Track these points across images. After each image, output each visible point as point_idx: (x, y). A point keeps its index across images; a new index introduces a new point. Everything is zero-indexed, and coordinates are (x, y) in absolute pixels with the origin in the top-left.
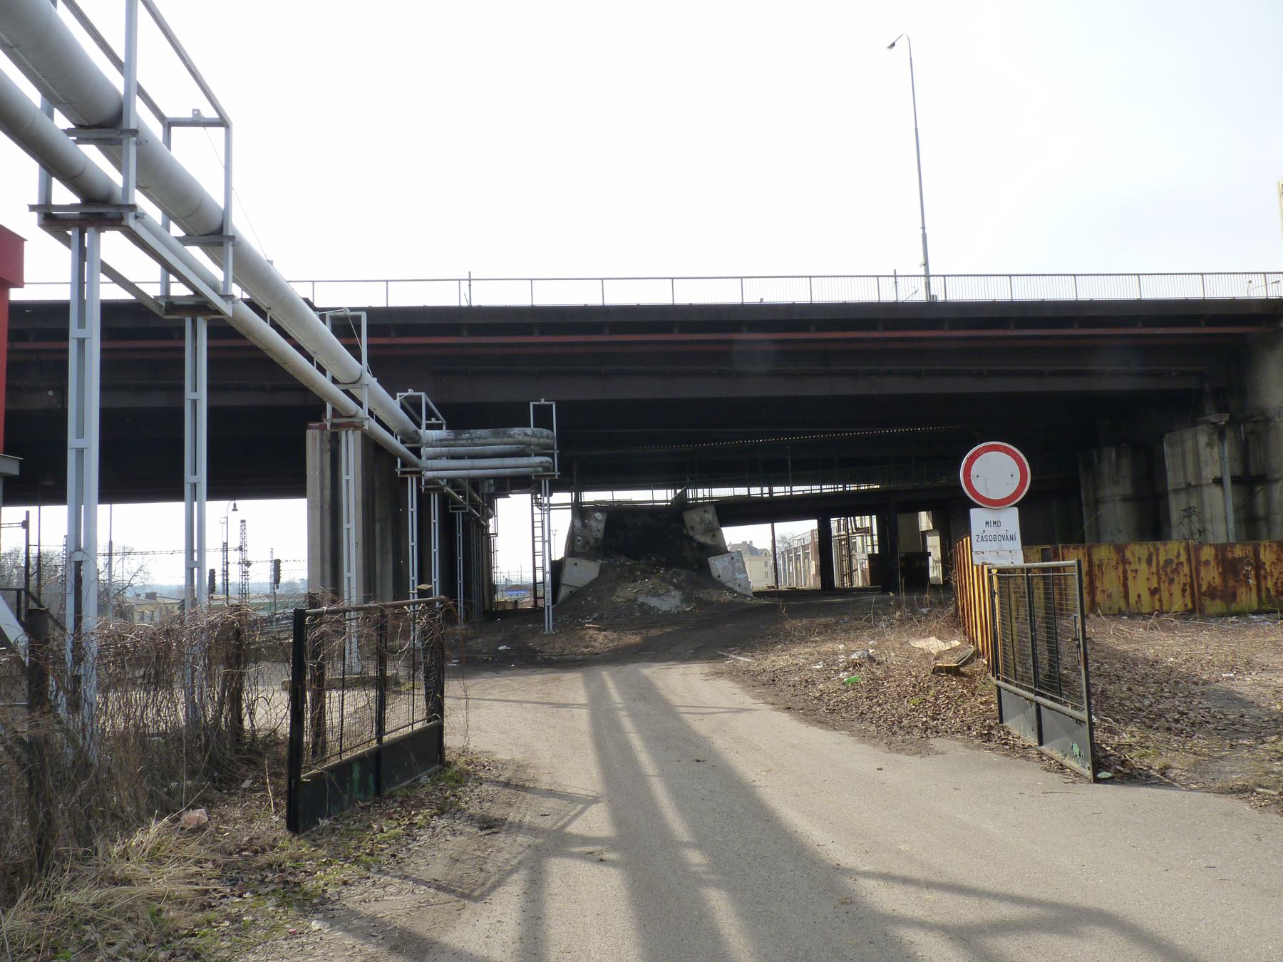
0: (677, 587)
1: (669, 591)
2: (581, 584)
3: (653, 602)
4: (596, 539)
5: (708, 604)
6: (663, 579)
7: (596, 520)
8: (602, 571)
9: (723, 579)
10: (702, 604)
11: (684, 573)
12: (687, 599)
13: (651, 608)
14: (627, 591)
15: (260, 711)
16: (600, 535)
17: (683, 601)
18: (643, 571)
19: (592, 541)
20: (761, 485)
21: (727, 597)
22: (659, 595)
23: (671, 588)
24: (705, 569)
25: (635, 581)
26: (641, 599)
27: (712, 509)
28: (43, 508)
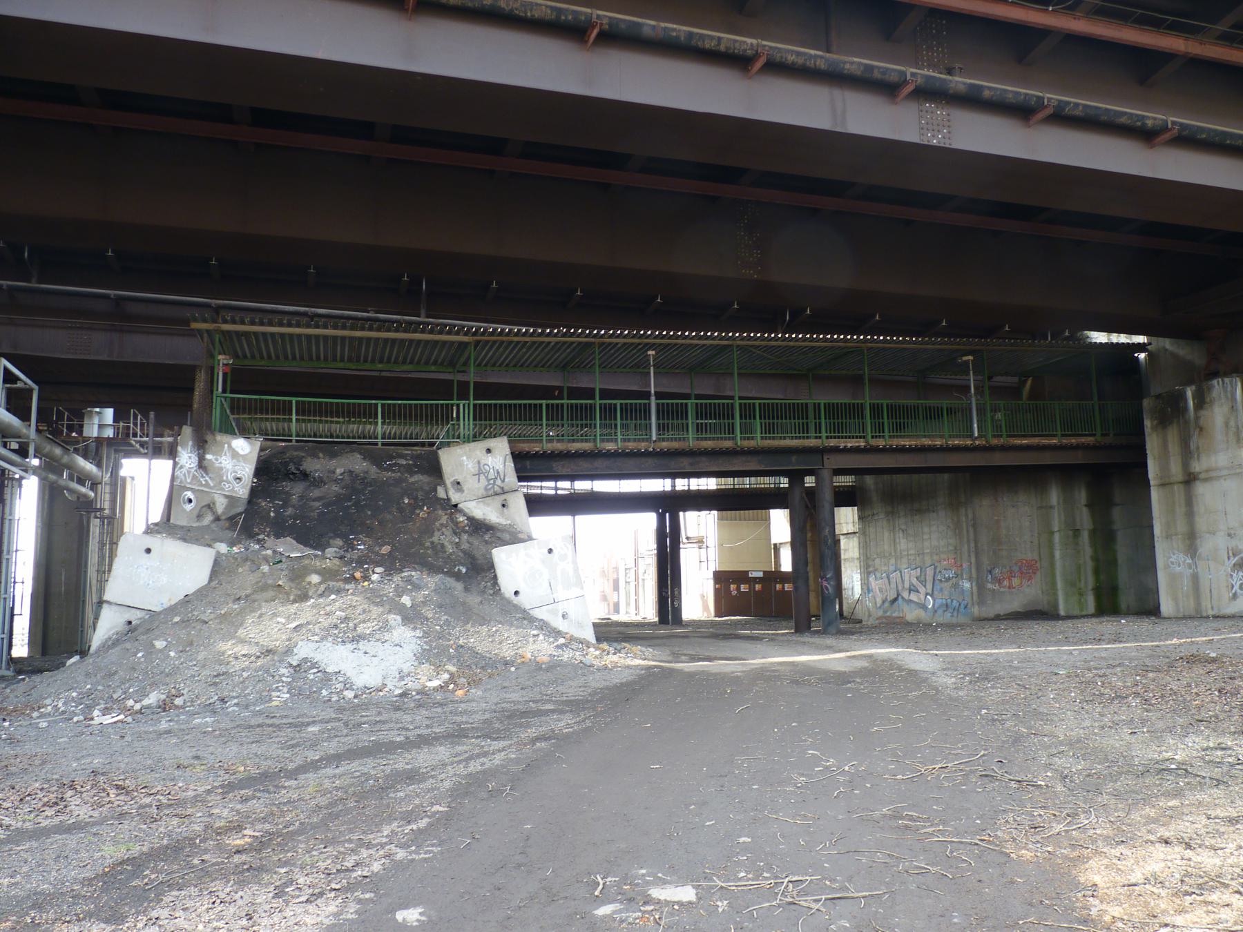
0: (411, 617)
1: (385, 627)
2: (158, 602)
3: (337, 658)
4: (232, 499)
5: (494, 666)
6: (375, 597)
7: (235, 455)
8: (218, 569)
9: (525, 601)
10: (478, 668)
11: (432, 581)
12: (431, 655)
13: (326, 678)
14: (271, 626)
15: (572, 609)
16: (242, 491)
17: (423, 657)
18: (327, 575)
19: (221, 505)
20: (535, 325)
21: (540, 648)
22: (357, 639)
23: (394, 619)
24: (480, 572)
25: (303, 597)
26: (304, 650)
27: (1123, 606)
28: (578, 518)
